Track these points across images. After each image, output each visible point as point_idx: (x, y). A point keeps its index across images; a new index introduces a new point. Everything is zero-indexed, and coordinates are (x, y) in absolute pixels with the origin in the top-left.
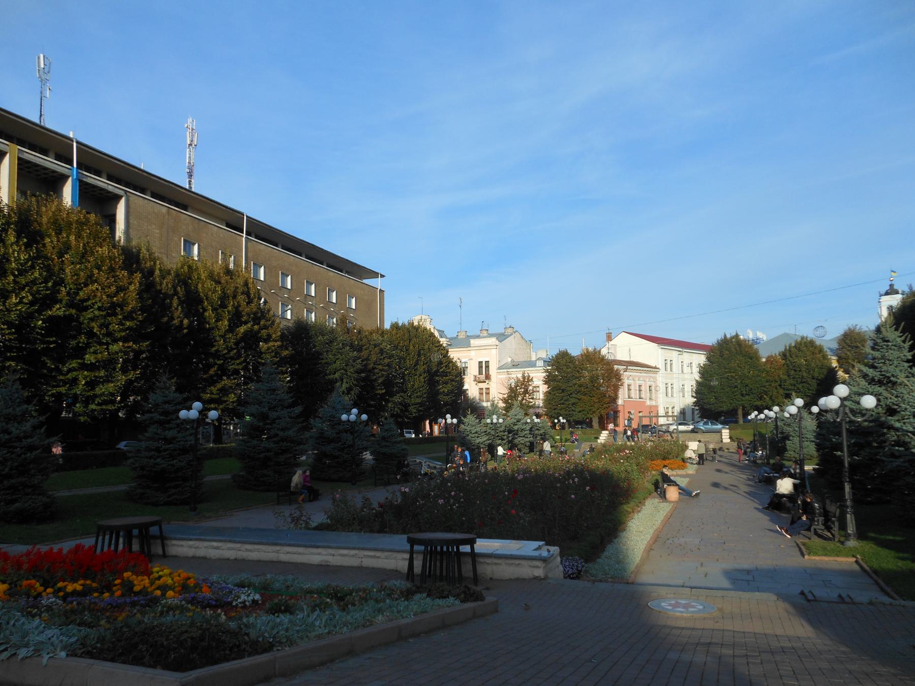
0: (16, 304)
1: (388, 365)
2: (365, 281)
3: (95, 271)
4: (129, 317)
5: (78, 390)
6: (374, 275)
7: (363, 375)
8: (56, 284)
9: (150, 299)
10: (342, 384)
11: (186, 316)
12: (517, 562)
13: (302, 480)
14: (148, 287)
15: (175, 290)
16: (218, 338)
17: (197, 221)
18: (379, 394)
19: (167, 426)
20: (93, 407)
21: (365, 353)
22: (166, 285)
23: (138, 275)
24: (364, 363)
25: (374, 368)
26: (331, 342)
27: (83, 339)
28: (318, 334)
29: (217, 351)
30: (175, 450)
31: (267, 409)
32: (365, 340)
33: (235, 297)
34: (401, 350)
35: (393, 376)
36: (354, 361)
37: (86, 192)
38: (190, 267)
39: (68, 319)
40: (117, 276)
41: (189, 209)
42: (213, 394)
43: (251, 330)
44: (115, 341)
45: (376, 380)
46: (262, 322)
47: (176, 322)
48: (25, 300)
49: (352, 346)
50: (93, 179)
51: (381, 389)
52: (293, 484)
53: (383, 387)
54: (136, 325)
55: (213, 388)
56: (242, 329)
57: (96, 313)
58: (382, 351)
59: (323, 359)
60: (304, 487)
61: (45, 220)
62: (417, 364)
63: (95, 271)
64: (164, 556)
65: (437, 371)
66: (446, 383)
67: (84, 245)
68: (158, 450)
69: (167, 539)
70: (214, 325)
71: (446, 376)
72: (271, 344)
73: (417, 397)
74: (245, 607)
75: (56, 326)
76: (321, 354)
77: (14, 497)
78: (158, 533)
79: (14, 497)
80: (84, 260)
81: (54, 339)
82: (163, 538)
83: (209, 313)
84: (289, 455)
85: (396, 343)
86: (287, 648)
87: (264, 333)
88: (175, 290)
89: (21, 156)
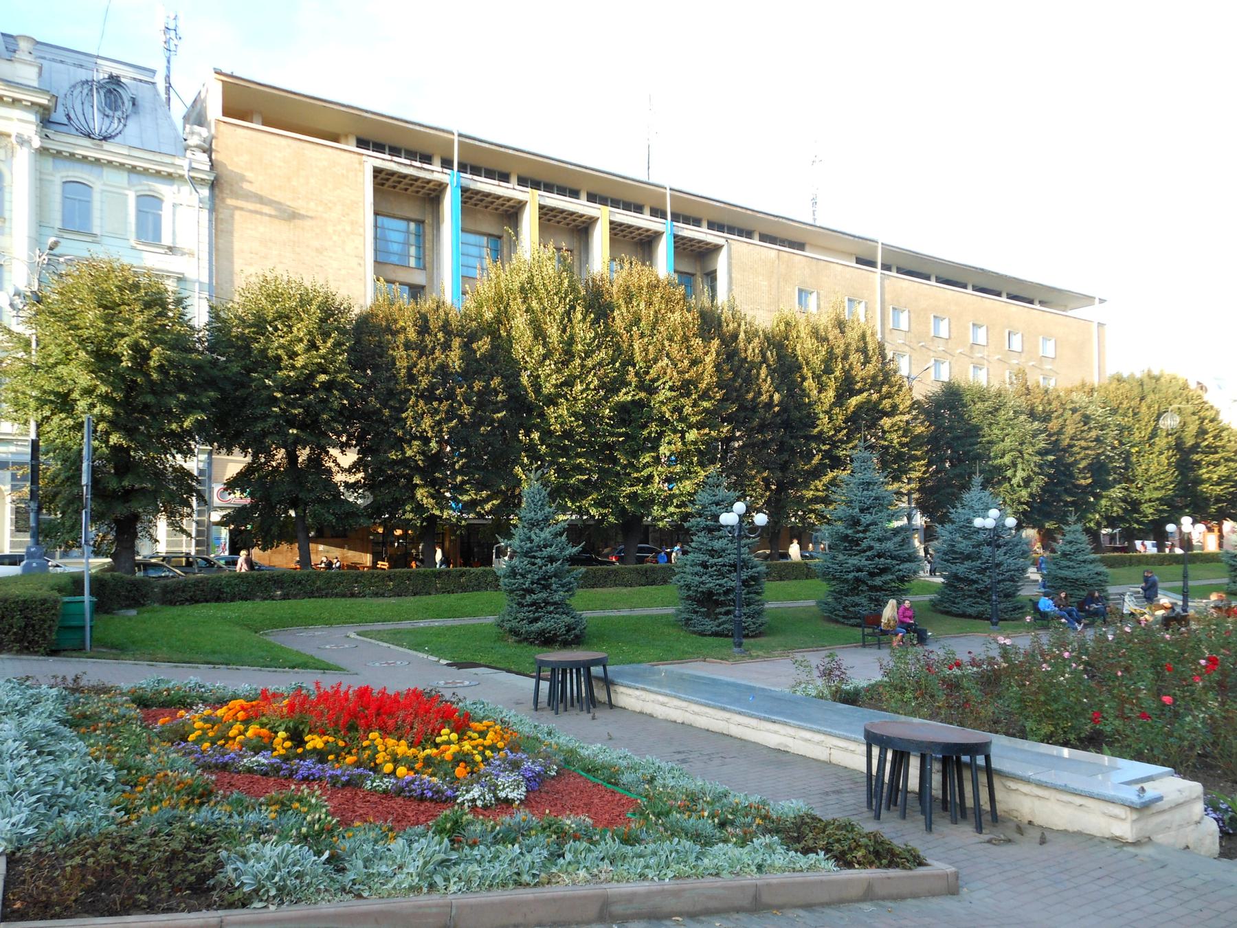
0: (582, 392)
1: (1097, 440)
2: (1070, 313)
3: (666, 343)
4: (705, 396)
5: (653, 488)
6: (1087, 300)
7: (1051, 458)
8: (624, 365)
9: (730, 370)
10: (1015, 471)
11: (777, 390)
12: (1078, 800)
13: (895, 613)
14: (730, 353)
15: (764, 356)
16: (821, 416)
17: (815, 261)
18: (1081, 485)
19: (716, 533)
20: (671, 509)
21: (1054, 425)
22: (752, 351)
23: (716, 343)
24: (1053, 439)
25: (1070, 446)
26: (997, 410)
27: (653, 427)
28: (976, 400)
29: (821, 432)
30: (724, 565)
31: (857, 510)
32: (1055, 404)
33: (845, 357)
34: (1125, 415)
35: (1108, 457)
36: (1034, 436)
37: (683, 247)
38: (787, 324)
39: (638, 405)
40: (692, 346)
41: (807, 247)
42: (818, 490)
43: (868, 401)
44: (690, 427)
45: (1076, 462)
46: (884, 389)
47: (764, 398)
48: (592, 386)
49: (1032, 415)
50: (689, 231)
51: (1085, 478)
52: (884, 620)
53: (1088, 475)
54: (713, 405)
55: (817, 482)
56: (854, 401)
57: (669, 394)
58: (1086, 419)
59: (983, 436)
60: (902, 623)
61: (615, 289)
62: (1154, 434)
63: (666, 343)
64: (611, 706)
65: (1197, 445)
66: (1216, 464)
67: (656, 312)
68: (704, 565)
69: (613, 683)
70: (815, 398)
71: (1216, 452)
72: (897, 418)
73: (1156, 489)
74: (474, 808)
75: (625, 413)
76: (981, 429)
77: (536, 615)
78: (602, 675)
79: (536, 615)
80: (655, 332)
81: (295, 432)
82: (608, 683)
83: (809, 384)
84: (891, 577)
85: (1115, 405)
86: (272, 908)
87: (886, 404)
88: (764, 356)
89: (613, 219)
